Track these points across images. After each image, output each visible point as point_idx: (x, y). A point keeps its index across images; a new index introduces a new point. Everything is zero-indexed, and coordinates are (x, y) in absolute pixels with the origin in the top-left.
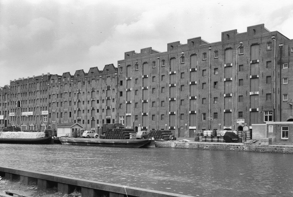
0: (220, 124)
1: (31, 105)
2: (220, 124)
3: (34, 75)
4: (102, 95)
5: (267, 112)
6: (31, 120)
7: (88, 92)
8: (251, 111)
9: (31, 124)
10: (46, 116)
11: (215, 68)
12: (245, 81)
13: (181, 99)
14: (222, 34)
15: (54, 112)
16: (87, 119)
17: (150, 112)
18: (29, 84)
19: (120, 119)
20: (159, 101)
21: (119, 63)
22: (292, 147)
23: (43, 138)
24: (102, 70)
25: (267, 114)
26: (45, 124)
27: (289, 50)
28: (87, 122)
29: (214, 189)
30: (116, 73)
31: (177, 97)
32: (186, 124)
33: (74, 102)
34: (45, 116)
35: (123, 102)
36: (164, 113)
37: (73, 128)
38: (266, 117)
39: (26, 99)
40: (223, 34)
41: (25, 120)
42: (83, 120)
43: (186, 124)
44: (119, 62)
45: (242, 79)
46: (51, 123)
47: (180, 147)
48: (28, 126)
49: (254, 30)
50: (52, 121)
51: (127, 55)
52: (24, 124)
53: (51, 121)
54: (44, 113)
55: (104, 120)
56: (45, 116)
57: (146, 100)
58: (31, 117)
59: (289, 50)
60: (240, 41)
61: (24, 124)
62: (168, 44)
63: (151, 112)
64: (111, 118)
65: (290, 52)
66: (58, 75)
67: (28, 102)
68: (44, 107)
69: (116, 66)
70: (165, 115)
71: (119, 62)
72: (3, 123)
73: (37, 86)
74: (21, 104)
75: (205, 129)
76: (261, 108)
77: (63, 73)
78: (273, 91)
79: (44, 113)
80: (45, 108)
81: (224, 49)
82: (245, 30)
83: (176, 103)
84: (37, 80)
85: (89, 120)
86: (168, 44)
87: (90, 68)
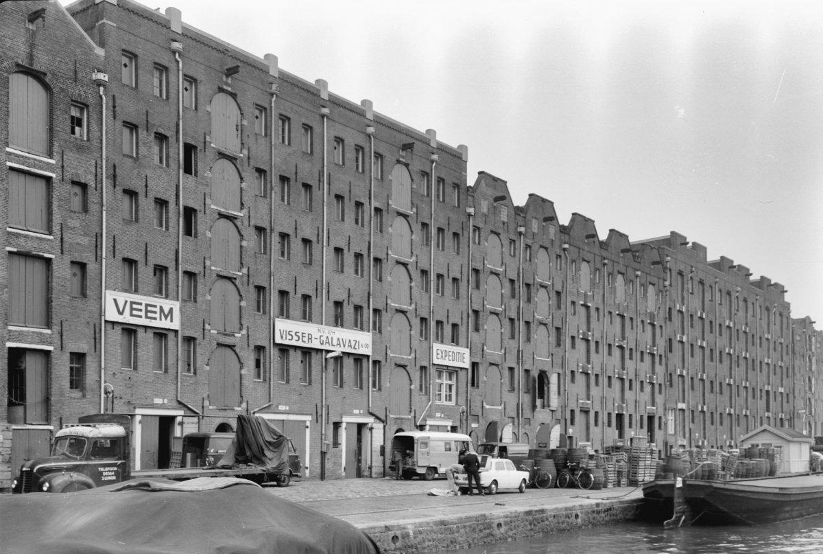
1: (346, 284)
6: (275, 380)
9: (351, 414)
10: (450, 375)
15: (498, 360)
24: (472, 185)
26: (448, 417)
29: (653, 536)
34: (445, 375)
41: (296, 382)
46: (480, 414)
47: (641, 471)
50: (487, 407)
52: (282, 408)
53: (479, 404)
54: (447, 353)
56: (445, 375)
58: (349, 363)
61: (282, 408)
64: (590, 406)
66: (635, 237)
72: (609, 425)
79: (447, 353)
80: (448, 329)
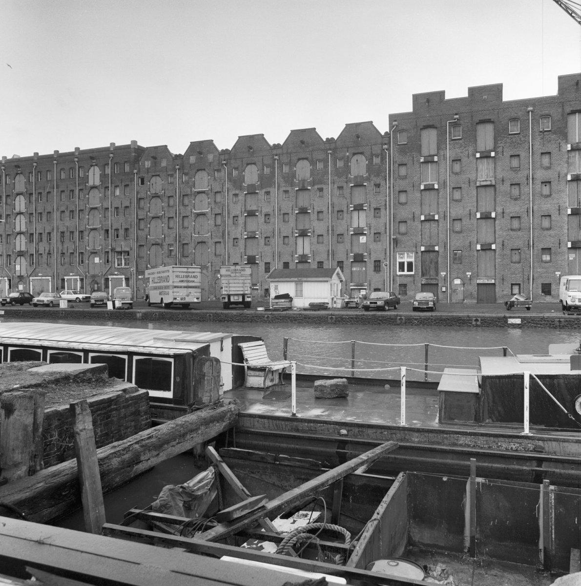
3: (55, 150)
8: (570, 247)
9: (69, 276)
16: (333, 259)
17: (503, 241)
18: (59, 169)
19: (399, 260)
22: (10, 316)
33: (231, 216)
35: (411, 216)
36: (552, 245)
39: (49, 209)
42: (266, 263)
44: (393, 118)
48: (58, 279)
61: (71, 274)
62: (560, 78)
63: (506, 241)
67: (56, 215)
68: (72, 232)
71: (393, 118)
73: (16, 182)
74: (328, 203)
75: (380, 289)
82: (465, 94)
84: (92, 158)
86: (560, 78)
87: (239, 137)
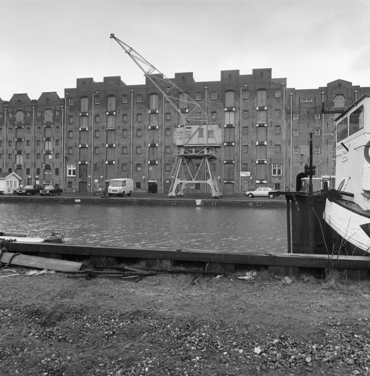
0: (220, 177)
2: (220, 177)
4: (35, 133)
5: (276, 165)
7: (9, 128)
11: (213, 111)
12: (251, 129)
13: (166, 145)
14: (221, 73)
19: (68, 169)
20: (132, 147)
21: (68, 92)
23: (10, 194)
25: (276, 167)
27: (300, 100)
28: (36, 172)
30: (62, 105)
31: (160, 142)
32: (102, 176)
35: (74, 145)
37: (8, 180)
38: (70, 171)
40: (78, 80)
43: (102, 176)
44: (67, 91)
45: (247, 126)
49: (183, 78)
51: (81, 82)
55: (11, 169)
57: (113, 145)
59: (300, 100)
60: (245, 84)
63: (120, 160)
65: (301, 102)
69: (62, 95)
70: (142, 164)
71: (67, 91)
76: (269, 160)
77: (14, 94)
78: (282, 143)
81: (224, 91)
82: (102, 80)
83: (159, 150)
85: (38, 169)
